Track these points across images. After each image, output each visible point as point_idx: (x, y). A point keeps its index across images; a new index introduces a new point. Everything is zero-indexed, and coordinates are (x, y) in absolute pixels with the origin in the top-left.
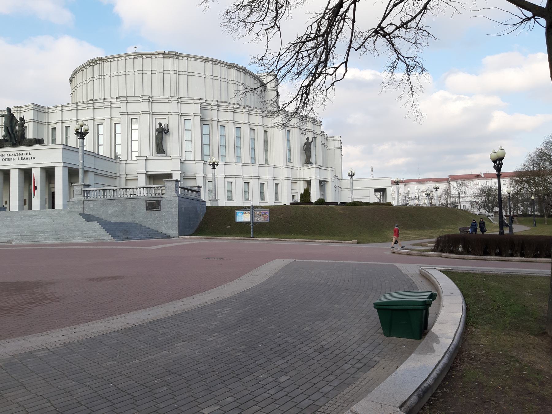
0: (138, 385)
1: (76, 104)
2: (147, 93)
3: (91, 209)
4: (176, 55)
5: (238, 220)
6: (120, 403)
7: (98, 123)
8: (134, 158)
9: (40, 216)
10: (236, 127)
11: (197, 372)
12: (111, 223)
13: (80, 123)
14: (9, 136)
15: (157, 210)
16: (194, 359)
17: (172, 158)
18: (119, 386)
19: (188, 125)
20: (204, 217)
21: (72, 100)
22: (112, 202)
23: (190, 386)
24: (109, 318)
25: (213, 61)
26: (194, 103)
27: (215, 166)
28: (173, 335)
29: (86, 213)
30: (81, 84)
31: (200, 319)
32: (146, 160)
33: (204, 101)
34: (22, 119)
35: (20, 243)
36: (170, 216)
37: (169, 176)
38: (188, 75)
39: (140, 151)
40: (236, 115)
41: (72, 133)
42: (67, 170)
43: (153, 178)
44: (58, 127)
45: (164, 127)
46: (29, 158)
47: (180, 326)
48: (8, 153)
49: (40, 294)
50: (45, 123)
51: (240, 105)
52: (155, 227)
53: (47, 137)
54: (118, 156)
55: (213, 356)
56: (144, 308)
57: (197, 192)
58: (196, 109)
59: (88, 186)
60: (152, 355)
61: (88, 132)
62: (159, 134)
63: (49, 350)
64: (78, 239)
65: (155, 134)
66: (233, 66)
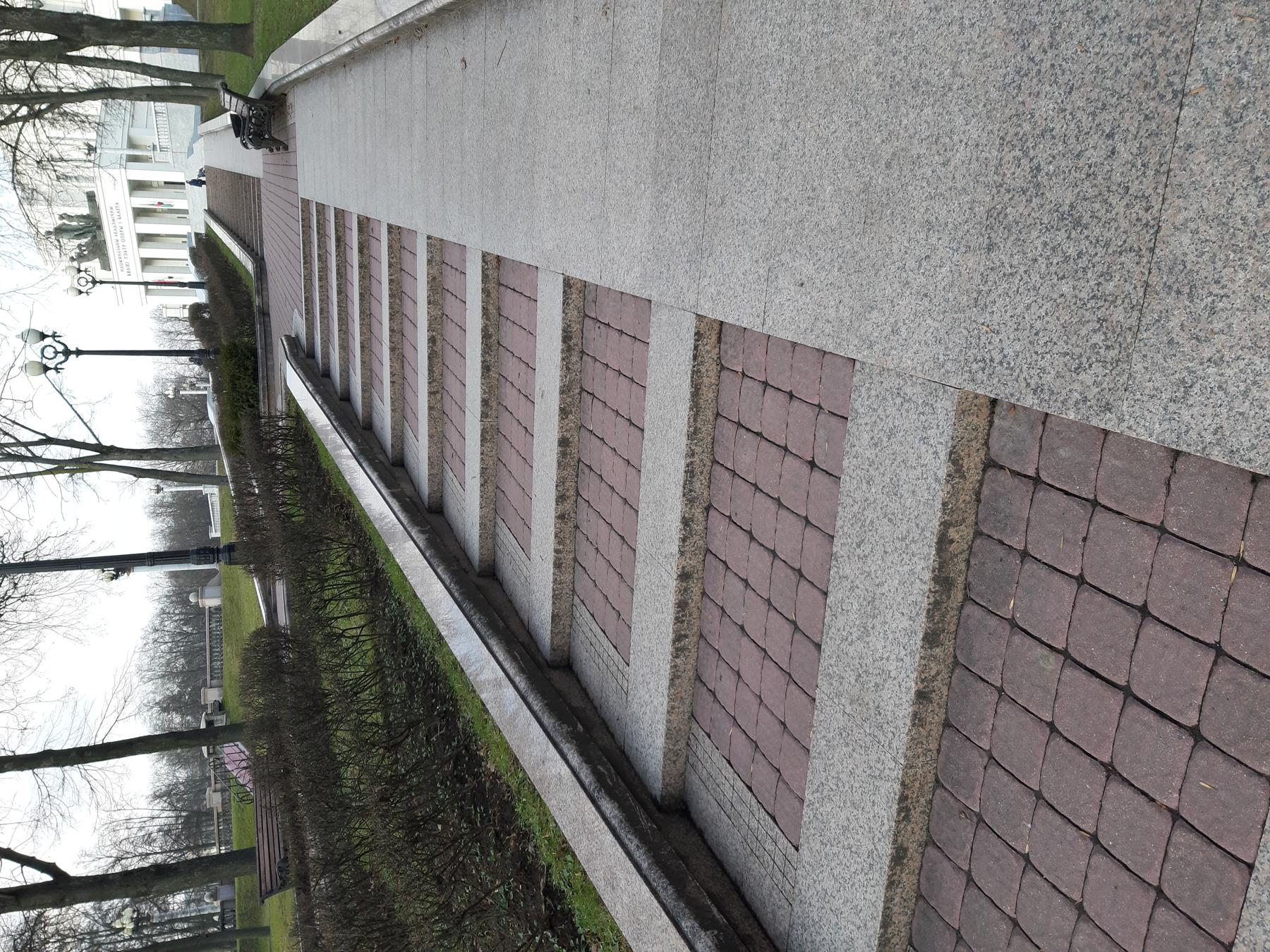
34: (61, 217)
48: (113, 235)
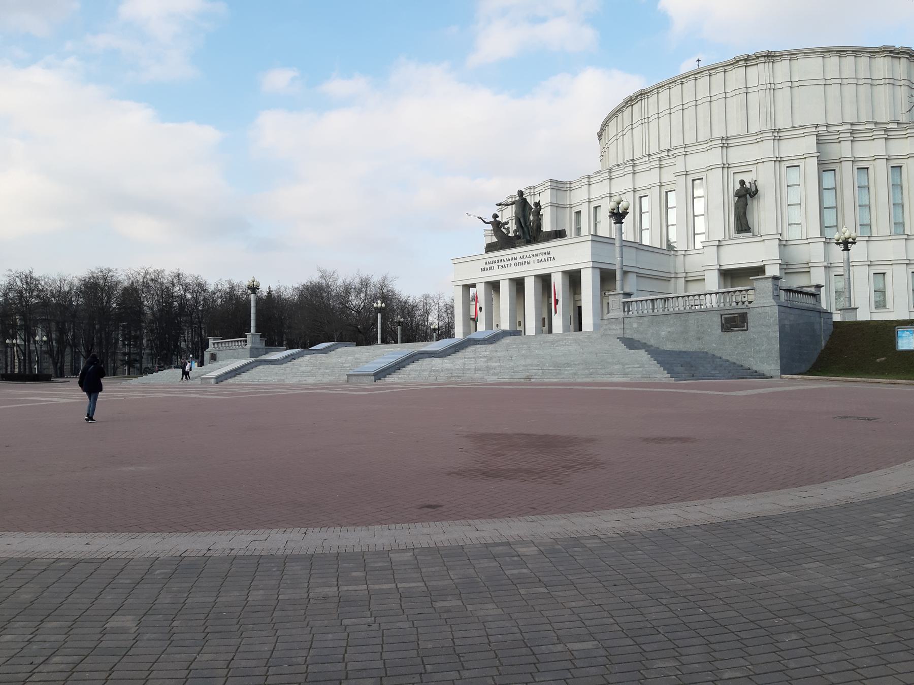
0: (745, 620)
1: (608, 171)
2: (719, 132)
3: (634, 330)
4: (770, 56)
5: (902, 347)
6: (718, 643)
7: (596, 206)
8: (699, 245)
9: (565, 342)
10: (892, 167)
11: (852, 620)
12: (665, 351)
13: (616, 199)
14: (521, 231)
15: (741, 331)
16: (842, 595)
17: (764, 238)
18: (716, 616)
19: (794, 176)
20: (828, 342)
21: (602, 165)
22: (666, 318)
23: (841, 642)
24: (682, 503)
25: (841, 52)
26: (805, 134)
27: (849, 245)
28: (797, 547)
29: (628, 337)
30: (615, 138)
31: (843, 526)
32: (718, 246)
33: (825, 128)
34: (537, 204)
35: (541, 381)
36: (765, 339)
37: (760, 270)
38: (791, 87)
39: (708, 232)
40: (891, 142)
41: (604, 215)
42: (598, 272)
43: (730, 275)
44: (584, 209)
45: (748, 186)
46: (548, 259)
47: (807, 534)
49: (578, 455)
50: (566, 206)
51: (899, 123)
52: (737, 360)
53: (569, 227)
54: (672, 245)
55: (882, 597)
56: (737, 495)
57: (814, 295)
58: (809, 144)
59: (629, 295)
60: (763, 575)
61: (628, 211)
62: (741, 199)
63: (600, 539)
64: (617, 376)
65: (732, 199)
66: (884, 51)
